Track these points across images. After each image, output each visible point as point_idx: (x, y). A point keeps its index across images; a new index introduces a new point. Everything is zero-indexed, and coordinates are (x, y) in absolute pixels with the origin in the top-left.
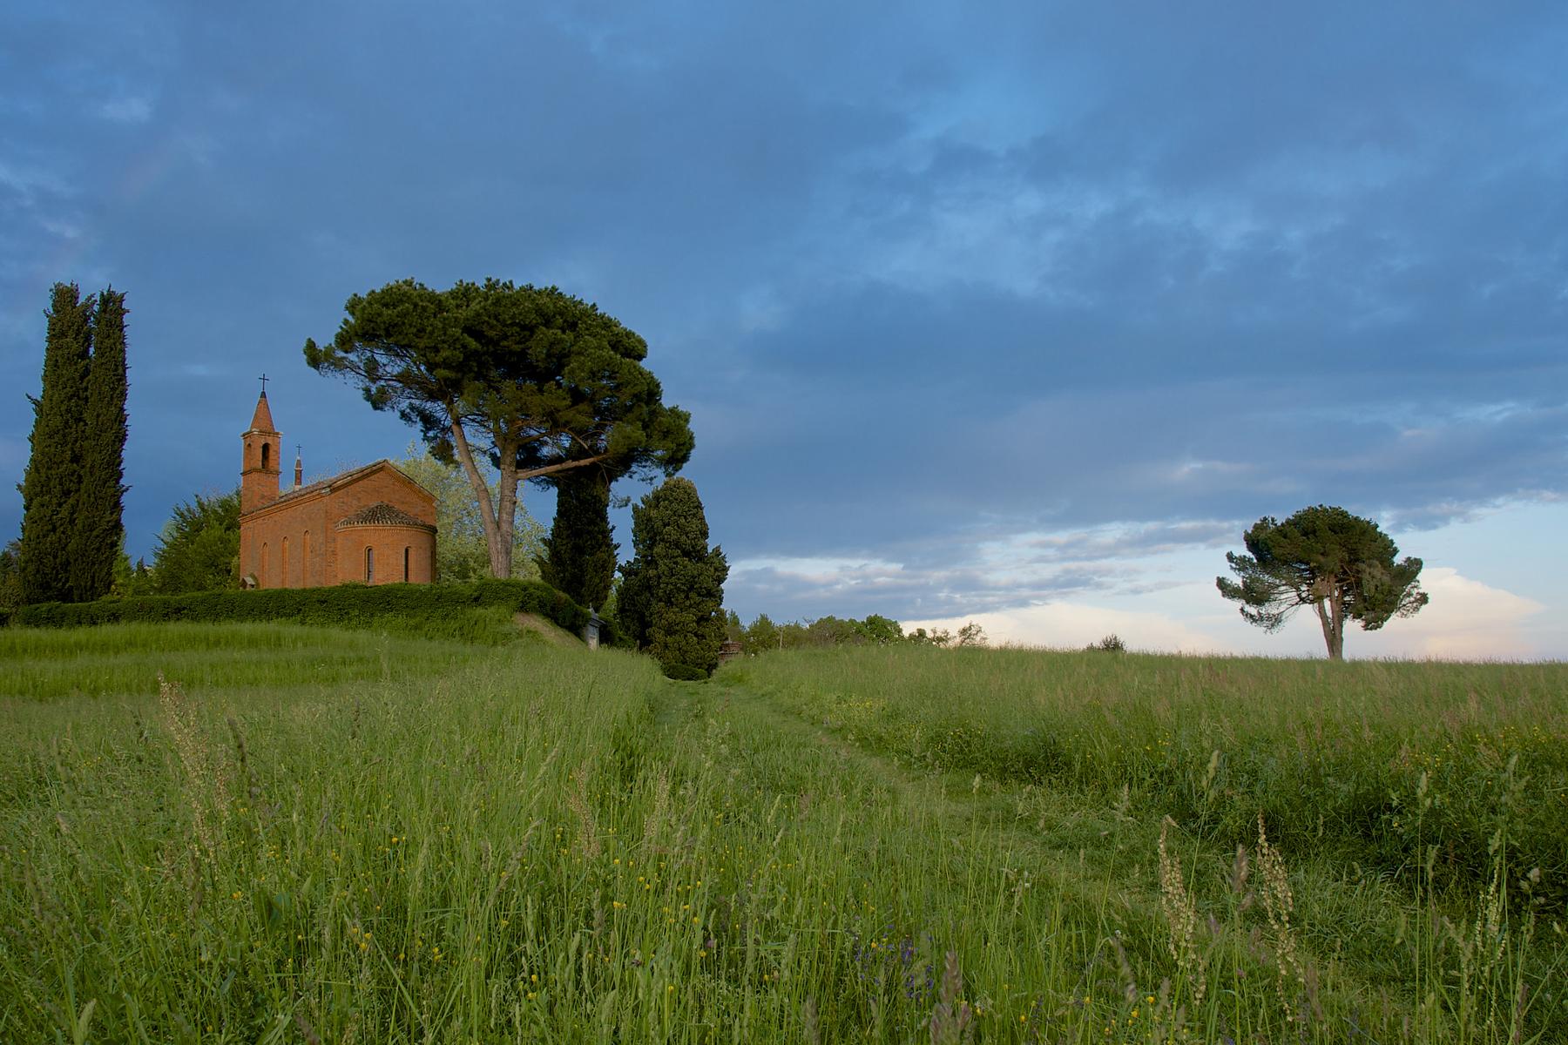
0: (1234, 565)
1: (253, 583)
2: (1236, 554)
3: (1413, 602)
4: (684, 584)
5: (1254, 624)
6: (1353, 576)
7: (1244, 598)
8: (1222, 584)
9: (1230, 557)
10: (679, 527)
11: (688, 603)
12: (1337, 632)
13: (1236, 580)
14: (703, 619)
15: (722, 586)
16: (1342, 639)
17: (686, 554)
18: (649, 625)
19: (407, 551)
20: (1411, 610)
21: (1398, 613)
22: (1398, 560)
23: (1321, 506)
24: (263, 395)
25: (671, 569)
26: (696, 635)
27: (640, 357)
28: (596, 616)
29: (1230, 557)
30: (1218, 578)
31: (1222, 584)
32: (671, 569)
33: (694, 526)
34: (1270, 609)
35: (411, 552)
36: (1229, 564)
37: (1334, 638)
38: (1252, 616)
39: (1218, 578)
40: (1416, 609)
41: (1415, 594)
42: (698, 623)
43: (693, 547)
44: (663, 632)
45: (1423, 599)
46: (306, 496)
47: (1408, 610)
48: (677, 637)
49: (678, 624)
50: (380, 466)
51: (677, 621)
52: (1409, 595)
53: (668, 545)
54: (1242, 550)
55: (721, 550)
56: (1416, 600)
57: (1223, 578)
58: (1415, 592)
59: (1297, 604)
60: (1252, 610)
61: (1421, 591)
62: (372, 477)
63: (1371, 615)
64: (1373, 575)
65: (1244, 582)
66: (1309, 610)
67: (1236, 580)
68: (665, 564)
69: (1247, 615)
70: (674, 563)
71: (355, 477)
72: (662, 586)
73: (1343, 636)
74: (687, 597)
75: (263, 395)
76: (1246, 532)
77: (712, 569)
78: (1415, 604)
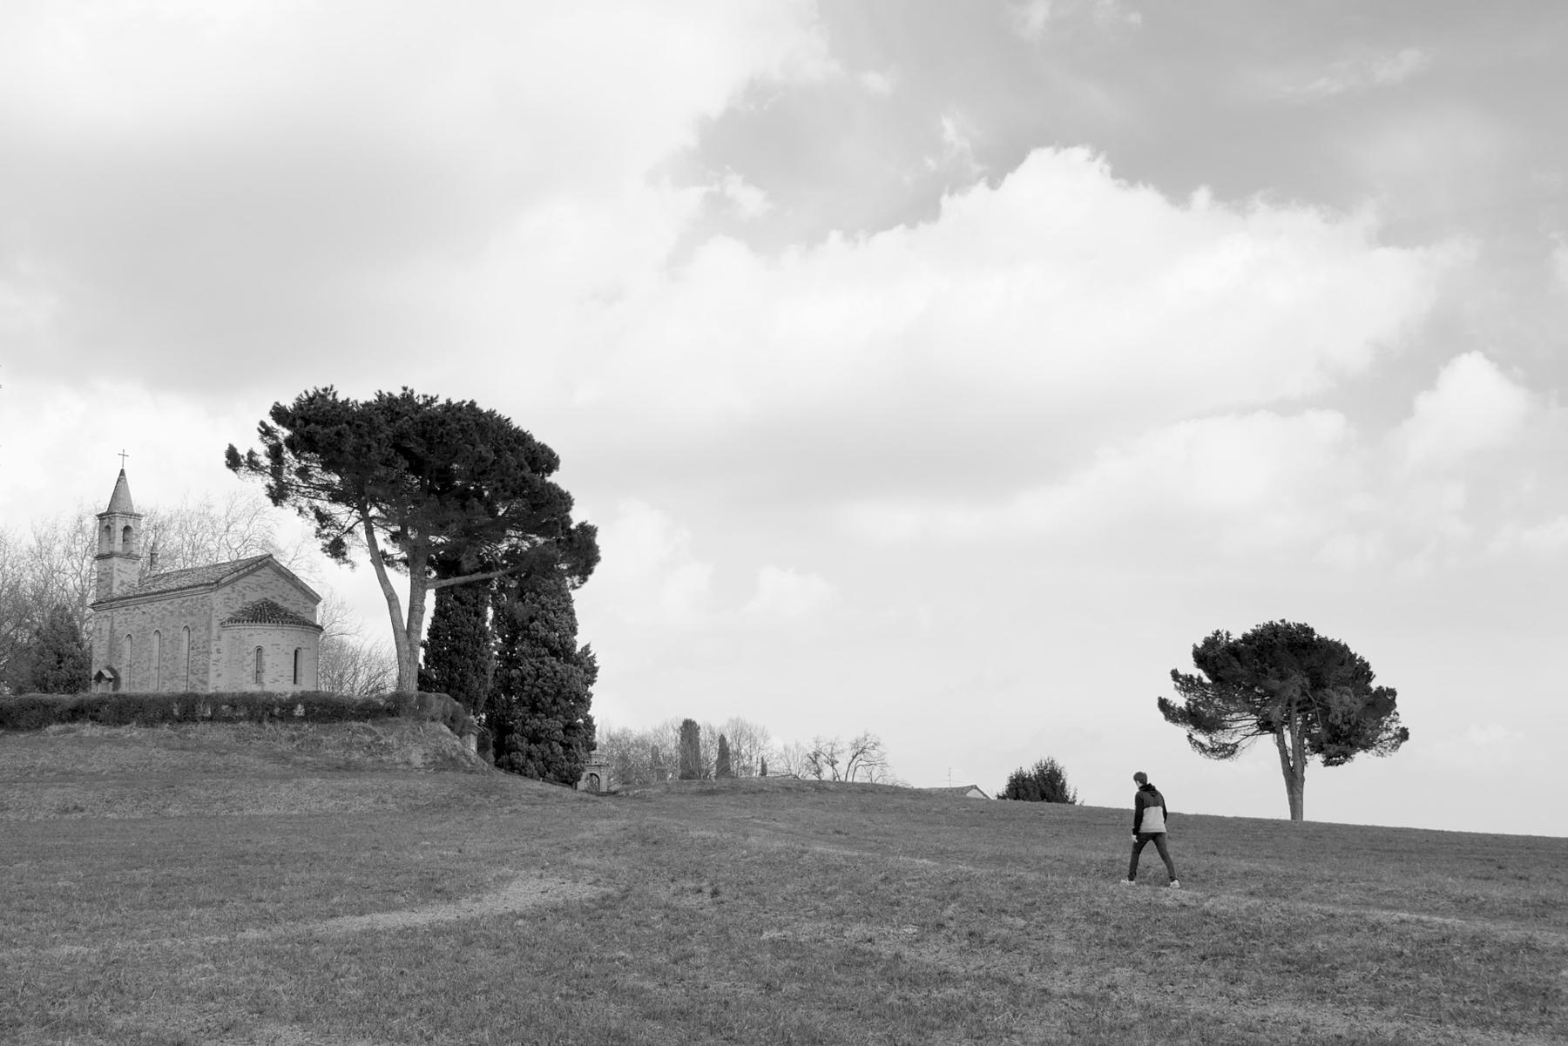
0: (1178, 684)
1: (112, 677)
2: (1181, 672)
3: (1393, 738)
4: (552, 688)
5: (1202, 754)
6: (1318, 705)
7: (1191, 722)
8: (1163, 704)
9: (1175, 675)
10: (547, 623)
11: (555, 709)
12: (1299, 770)
13: (1179, 701)
14: (570, 728)
15: (590, 689)
16: (1303, 780)
17: (554, 653)
18: (511, 730)
19: (296, 652)
20: (1389, 748)
21: (1373, 751)
22: (1374, 685)
23: (1283, 621)
24: (122, 473)
25: (538, 670)
26: (562, 744)
27: (549, 470)
28: (428, 714)
29: (1175, 675)
30: (1160, 698)
31: (1163, 704)
32: (538, 670)
33: (564, 622)
34: (1223, 737)
35: (303, 655)
36: (1174, 683)
37: (1294, 779)
38: (1202, 745)
39: (1160, 698)
40: (1396, 747)
41: (1394, 729)
42: (564, 731)
43: (561, 645)
44: (526, 740)
45: (1404, 735)
46: (199, 589)
47: (1385, 748)
48: (541, 746)
49: (543, 731)
50: (265, 561)
51: (542, 728)
52: (1388, 729)
53: (534, 642)
54: (1191, 669)
55: (590, 649)
56: (1396, 736)
57: (1165, 699)
58: (1394, 726)
59: (1253, 735)
60: (1201, 737)
61: (1401, 726)
62: (257, 573)
63: (1333, 748)
64: (1341, 701)
65: (1188, 704)
66: (1269, 739)
67: (1179, 701)
68: (530, 663)
69: (1195, 744)
70: (541, 663)
71: (241, 572)
72: (526, 688)
73: (1305, 775)
74: (554, 703)
75: (122, 473)
76: (1195, 646)
77: (582, 671)
78: (1393, 741)
